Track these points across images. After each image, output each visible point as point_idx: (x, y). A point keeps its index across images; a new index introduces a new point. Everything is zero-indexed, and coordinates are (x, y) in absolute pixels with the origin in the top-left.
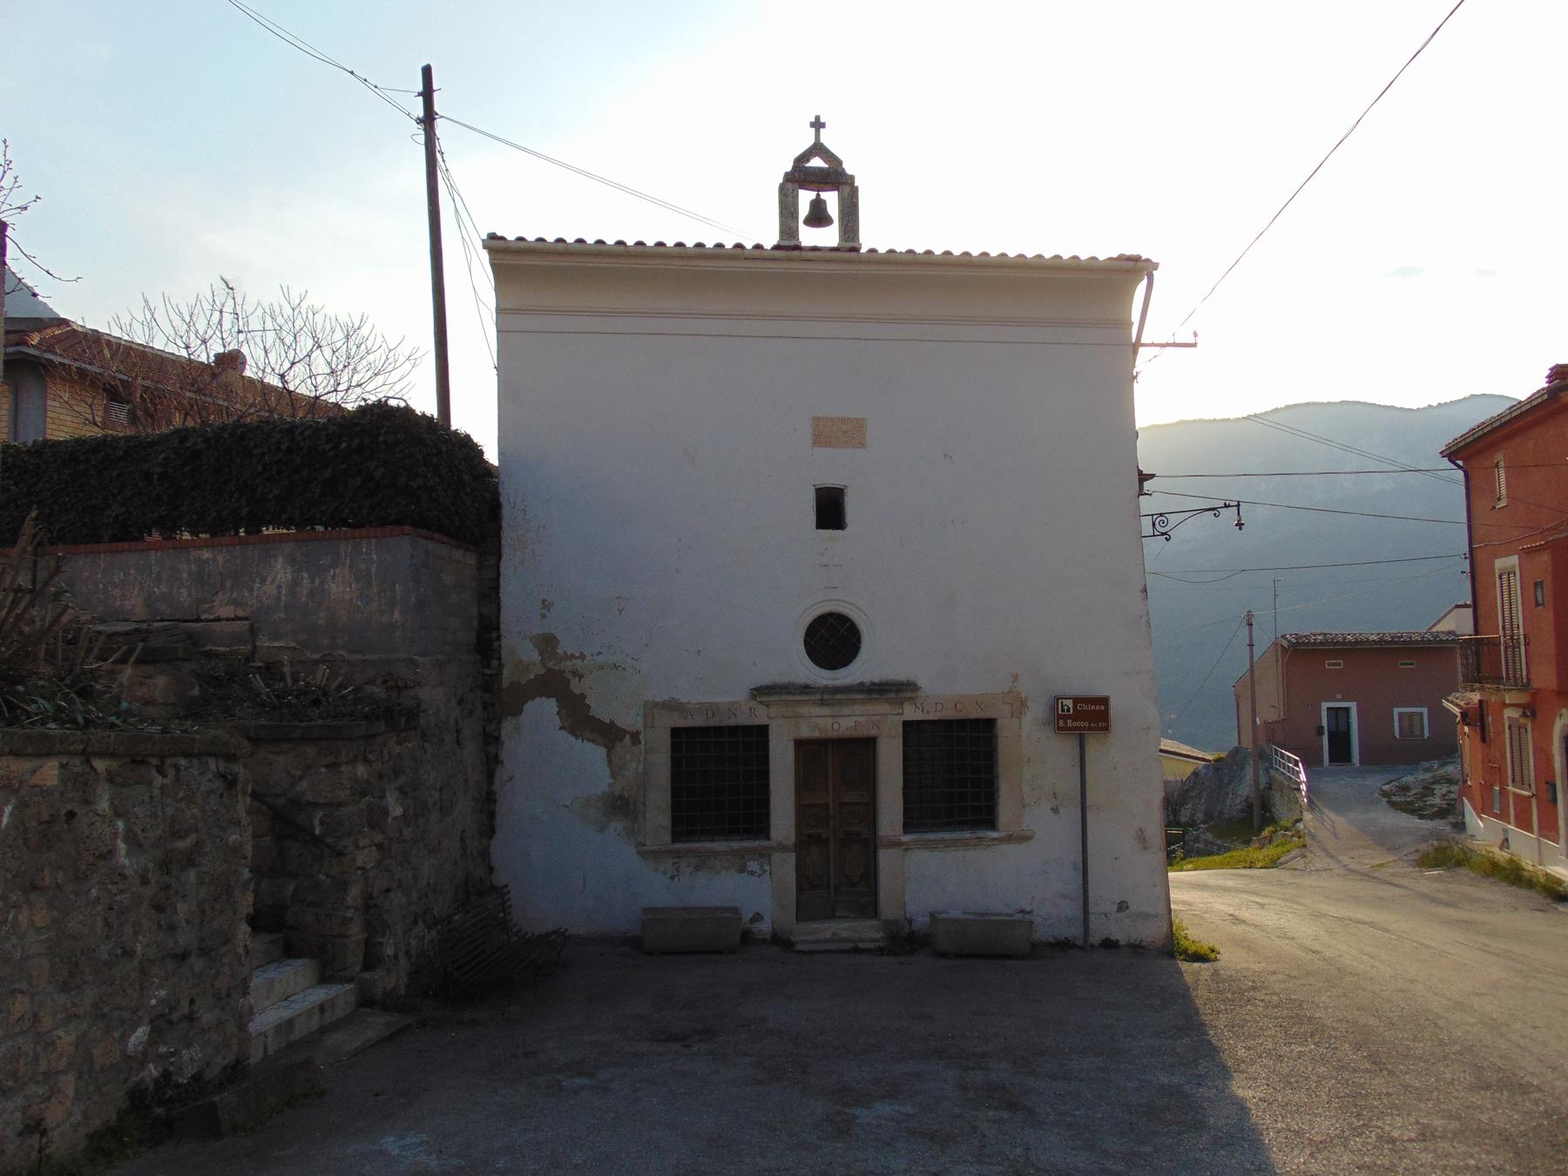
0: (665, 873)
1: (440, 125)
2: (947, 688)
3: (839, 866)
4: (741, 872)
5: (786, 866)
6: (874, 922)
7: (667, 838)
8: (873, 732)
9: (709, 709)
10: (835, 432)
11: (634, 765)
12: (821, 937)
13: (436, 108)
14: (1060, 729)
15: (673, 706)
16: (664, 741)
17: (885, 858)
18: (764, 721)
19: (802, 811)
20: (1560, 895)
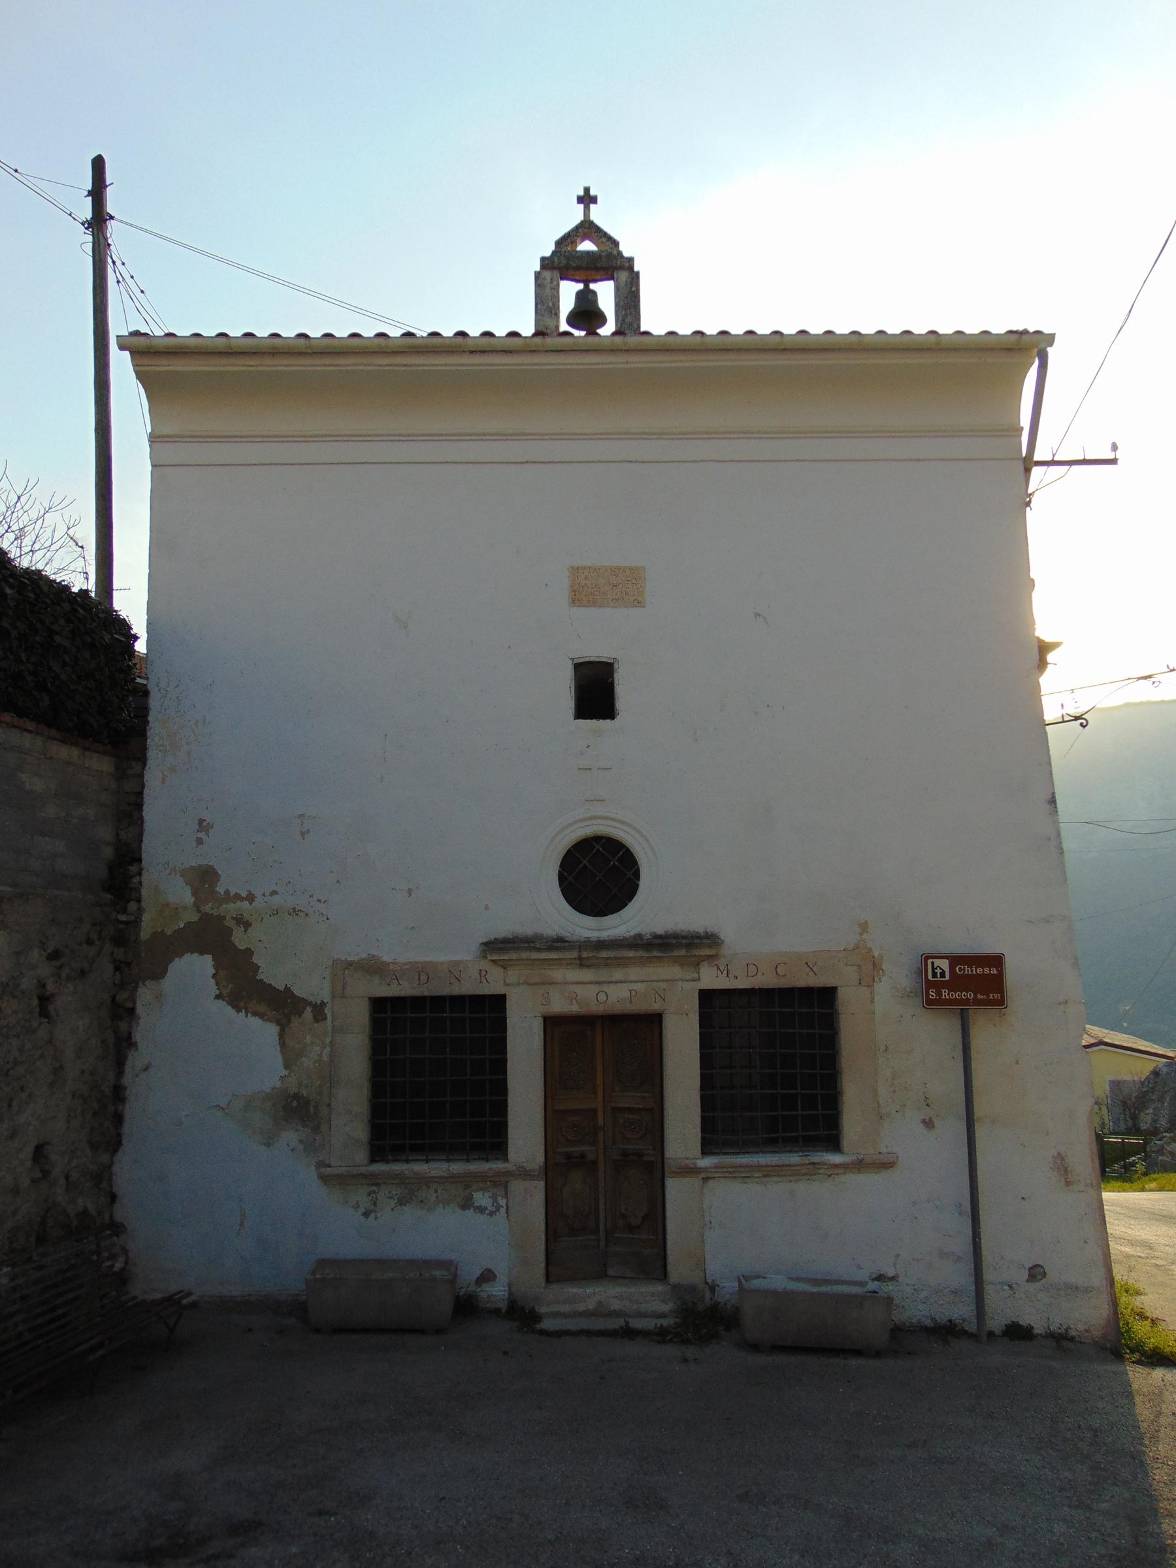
1: (112, 228)
2: (764, 941)
3: (607, 1204)
5: (531, 1200)
6: (659, 1288)
7: (361, 1156)
8: (656, 1006)
9: (421, 970)
10: (595, 587)
13: (110, 208)
14: (930, 1002)
15: (373, 967)
16: (359, 1017)
17: (675, 1189)
19: (555, 1118)
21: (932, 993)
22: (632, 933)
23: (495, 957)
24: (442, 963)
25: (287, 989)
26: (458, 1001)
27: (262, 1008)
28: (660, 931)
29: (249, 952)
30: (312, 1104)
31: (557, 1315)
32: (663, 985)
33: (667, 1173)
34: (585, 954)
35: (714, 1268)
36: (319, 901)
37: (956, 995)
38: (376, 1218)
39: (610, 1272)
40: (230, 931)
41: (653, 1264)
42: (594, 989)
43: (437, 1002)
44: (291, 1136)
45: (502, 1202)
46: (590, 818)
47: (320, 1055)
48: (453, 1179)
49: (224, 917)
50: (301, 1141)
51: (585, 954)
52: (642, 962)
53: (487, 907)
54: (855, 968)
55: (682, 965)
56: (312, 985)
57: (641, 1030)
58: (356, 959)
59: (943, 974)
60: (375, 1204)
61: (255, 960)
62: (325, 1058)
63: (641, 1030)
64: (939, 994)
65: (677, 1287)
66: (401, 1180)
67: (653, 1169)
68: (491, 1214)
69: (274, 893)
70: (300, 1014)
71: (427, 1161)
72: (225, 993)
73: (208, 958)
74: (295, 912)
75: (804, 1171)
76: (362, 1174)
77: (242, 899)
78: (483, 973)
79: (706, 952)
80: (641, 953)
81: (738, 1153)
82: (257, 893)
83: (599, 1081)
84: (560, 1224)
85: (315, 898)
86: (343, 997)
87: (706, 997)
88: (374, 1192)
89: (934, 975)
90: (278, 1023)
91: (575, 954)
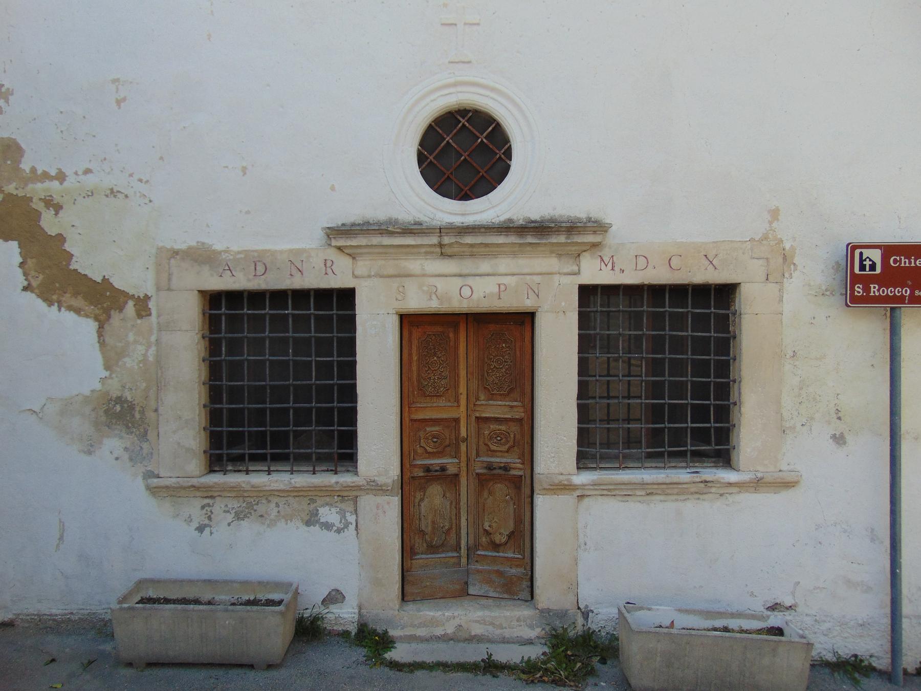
0: (189, 520)
2: (650, 244)
3: (469, 516)
4: (308, 523)
5: (384, 518)
6: (525, 612)
7: (194, 465)
8: (526, 303)
9: (258, 261)
11: (141, 349)
15: (201, 256)
17: (546, 509)
18: (338, 281)
19: (410, 429)
21: (859, 290)
22: (502, 218)
23: (341, 243)
24: (281, 252)
25: (105, 280)
26: (301, 296)
27: (79, 302)
28: (535, 216)
29: (61, 239)
30: (137, 409)
31: (412, 639)
32: (537, 279)
33: (536, 490)
34: (446, 240)
35: (588, 594)
36: (140, 180)
37: (889, 291)
38: (211, 533)
39: (471, 591)
40: (39, 214)
41: (520, 584)
42: (459, 282)
43: (279, 297)
44: (114, 444)
46: (455, 85)
47: (145, 355)
48: (297, 492)
49: (31, 199)
50: (126, 449)
51: (446, 240)
52: (514, 255)
53: (333, 188)
54: (761, 262)
55: (559, 256)
56: (134, 278)
57: (513, 328)
58: (183, 247)
59: (873, 267)
60: (210, 518)
61: (67, 247)
62: (151, 359)
63: (513, 328)
64: (867, 289)
65: (546, 613)
66: (238, 492)
67: (523, 487)
68: (339, 531)
69: (88, 171)
70: (121, 309)
71: (269, 472)
72: (35, 284)
73: (14, 245)
74: (113, 193)
75: (693, 490)
76: (193, 486)
77: (51, 178)
78: (329, 264)
79: (590, 238)
80: (513, 239)
81: (619, 468)
82: (69, 172)
83: (462, 389)
84: (417, 541)
85: (136, 177)
86: (169, 289)
87: (586, 292)
88: (208, 505)
89: (862, 267)
90: (96, 319)
91: (434, 240)
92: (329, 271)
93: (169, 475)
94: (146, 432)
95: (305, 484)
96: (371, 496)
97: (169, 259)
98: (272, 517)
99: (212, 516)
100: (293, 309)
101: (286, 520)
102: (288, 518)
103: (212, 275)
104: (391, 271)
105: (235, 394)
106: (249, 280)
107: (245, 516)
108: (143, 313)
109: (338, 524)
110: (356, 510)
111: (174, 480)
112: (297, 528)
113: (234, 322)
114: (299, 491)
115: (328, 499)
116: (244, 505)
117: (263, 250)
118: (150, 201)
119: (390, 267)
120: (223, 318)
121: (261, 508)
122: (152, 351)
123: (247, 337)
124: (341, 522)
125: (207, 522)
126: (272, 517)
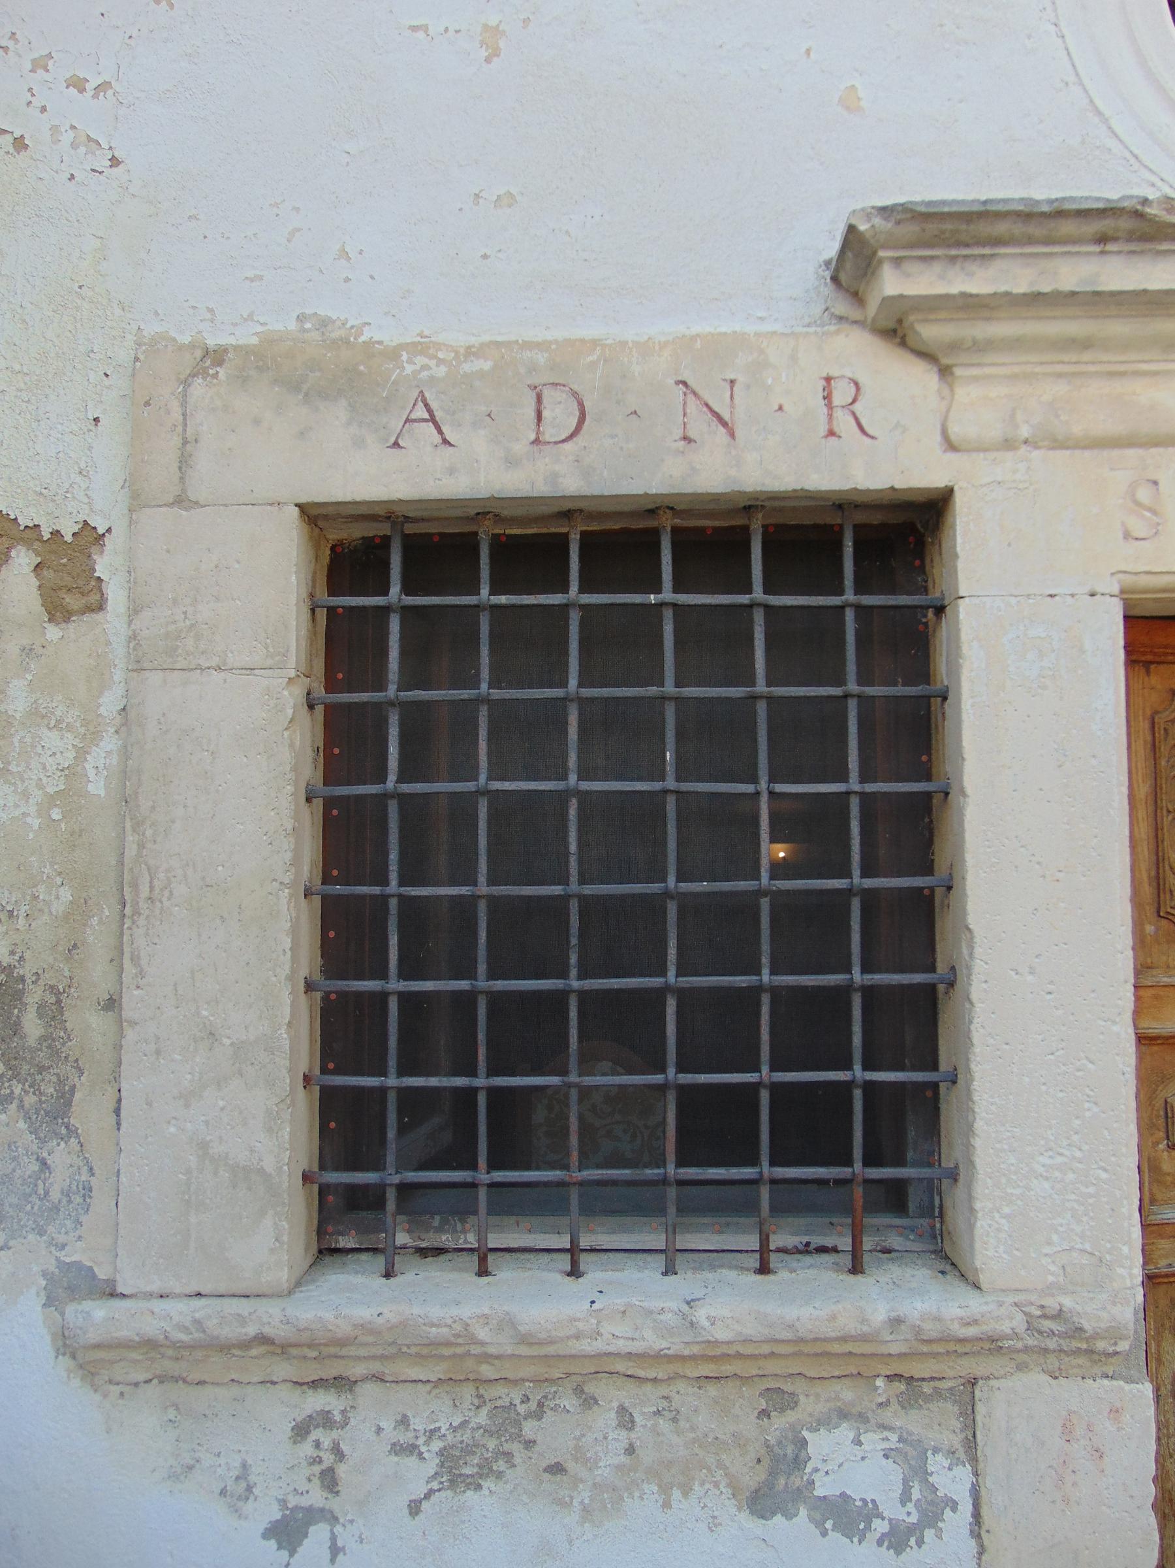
0: (240, 1490)
4: (762, 1502)
7: (272, 1234)
9: (551, 389)
11: (57, 746)
12: (884, 1349)
15: (327, 372)
16: (268, 600)
20: (1173, 1044)
24: (646, 349)
30: (34, 996)
38: (335, 1551)
45: (954, 1481)
47: (73, 774)
48: (713, 1364)
53: (850, 102)
58: (247, 336)
60: (329, 1481)
62: (97, 787)
66: (457, 1365)
68: (899, 1539)
76: (263, 1339)
78: (842, 395)
86: (181, 501)
88: (325, 1420)
92: (844, 423)
93: (156, 1286)
94: (65, 1097)
95: (751, 1329)
96: (1036, 1378)
97: (186, 383)
98: (603, 1472)
99: (342, 1470)
100: (676, 589)
101: (665, 1489)
102: (674, 1479)
103: (359, 443)
104: (1104, 423)
105: (432, 937)
106: (511, 462)
107: (486, 1470)
108: (72, 601)
109: (892, 1509)
110: (971, 1444)
111: (179, 1310)
112: (714, 1524)
113: (438, 643)
114: (726, 1357)
115: (847, 1393)
116: (482, 1418)
117: (569, 342)
118: (115, 162)
119: (1095, 405)
120: (395, 625)
121: (554, 1435)
122: (105, 751)
123: (487, 701)
124: (905, 1498)
125: (316, 1497)
126: (603, 1472)
